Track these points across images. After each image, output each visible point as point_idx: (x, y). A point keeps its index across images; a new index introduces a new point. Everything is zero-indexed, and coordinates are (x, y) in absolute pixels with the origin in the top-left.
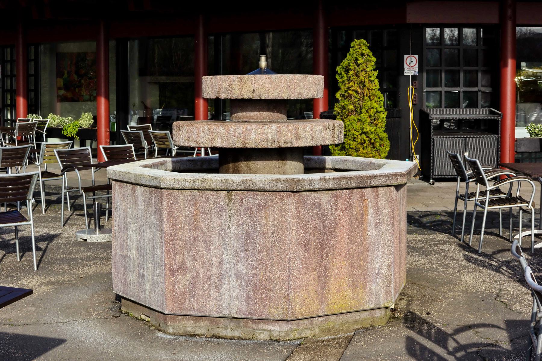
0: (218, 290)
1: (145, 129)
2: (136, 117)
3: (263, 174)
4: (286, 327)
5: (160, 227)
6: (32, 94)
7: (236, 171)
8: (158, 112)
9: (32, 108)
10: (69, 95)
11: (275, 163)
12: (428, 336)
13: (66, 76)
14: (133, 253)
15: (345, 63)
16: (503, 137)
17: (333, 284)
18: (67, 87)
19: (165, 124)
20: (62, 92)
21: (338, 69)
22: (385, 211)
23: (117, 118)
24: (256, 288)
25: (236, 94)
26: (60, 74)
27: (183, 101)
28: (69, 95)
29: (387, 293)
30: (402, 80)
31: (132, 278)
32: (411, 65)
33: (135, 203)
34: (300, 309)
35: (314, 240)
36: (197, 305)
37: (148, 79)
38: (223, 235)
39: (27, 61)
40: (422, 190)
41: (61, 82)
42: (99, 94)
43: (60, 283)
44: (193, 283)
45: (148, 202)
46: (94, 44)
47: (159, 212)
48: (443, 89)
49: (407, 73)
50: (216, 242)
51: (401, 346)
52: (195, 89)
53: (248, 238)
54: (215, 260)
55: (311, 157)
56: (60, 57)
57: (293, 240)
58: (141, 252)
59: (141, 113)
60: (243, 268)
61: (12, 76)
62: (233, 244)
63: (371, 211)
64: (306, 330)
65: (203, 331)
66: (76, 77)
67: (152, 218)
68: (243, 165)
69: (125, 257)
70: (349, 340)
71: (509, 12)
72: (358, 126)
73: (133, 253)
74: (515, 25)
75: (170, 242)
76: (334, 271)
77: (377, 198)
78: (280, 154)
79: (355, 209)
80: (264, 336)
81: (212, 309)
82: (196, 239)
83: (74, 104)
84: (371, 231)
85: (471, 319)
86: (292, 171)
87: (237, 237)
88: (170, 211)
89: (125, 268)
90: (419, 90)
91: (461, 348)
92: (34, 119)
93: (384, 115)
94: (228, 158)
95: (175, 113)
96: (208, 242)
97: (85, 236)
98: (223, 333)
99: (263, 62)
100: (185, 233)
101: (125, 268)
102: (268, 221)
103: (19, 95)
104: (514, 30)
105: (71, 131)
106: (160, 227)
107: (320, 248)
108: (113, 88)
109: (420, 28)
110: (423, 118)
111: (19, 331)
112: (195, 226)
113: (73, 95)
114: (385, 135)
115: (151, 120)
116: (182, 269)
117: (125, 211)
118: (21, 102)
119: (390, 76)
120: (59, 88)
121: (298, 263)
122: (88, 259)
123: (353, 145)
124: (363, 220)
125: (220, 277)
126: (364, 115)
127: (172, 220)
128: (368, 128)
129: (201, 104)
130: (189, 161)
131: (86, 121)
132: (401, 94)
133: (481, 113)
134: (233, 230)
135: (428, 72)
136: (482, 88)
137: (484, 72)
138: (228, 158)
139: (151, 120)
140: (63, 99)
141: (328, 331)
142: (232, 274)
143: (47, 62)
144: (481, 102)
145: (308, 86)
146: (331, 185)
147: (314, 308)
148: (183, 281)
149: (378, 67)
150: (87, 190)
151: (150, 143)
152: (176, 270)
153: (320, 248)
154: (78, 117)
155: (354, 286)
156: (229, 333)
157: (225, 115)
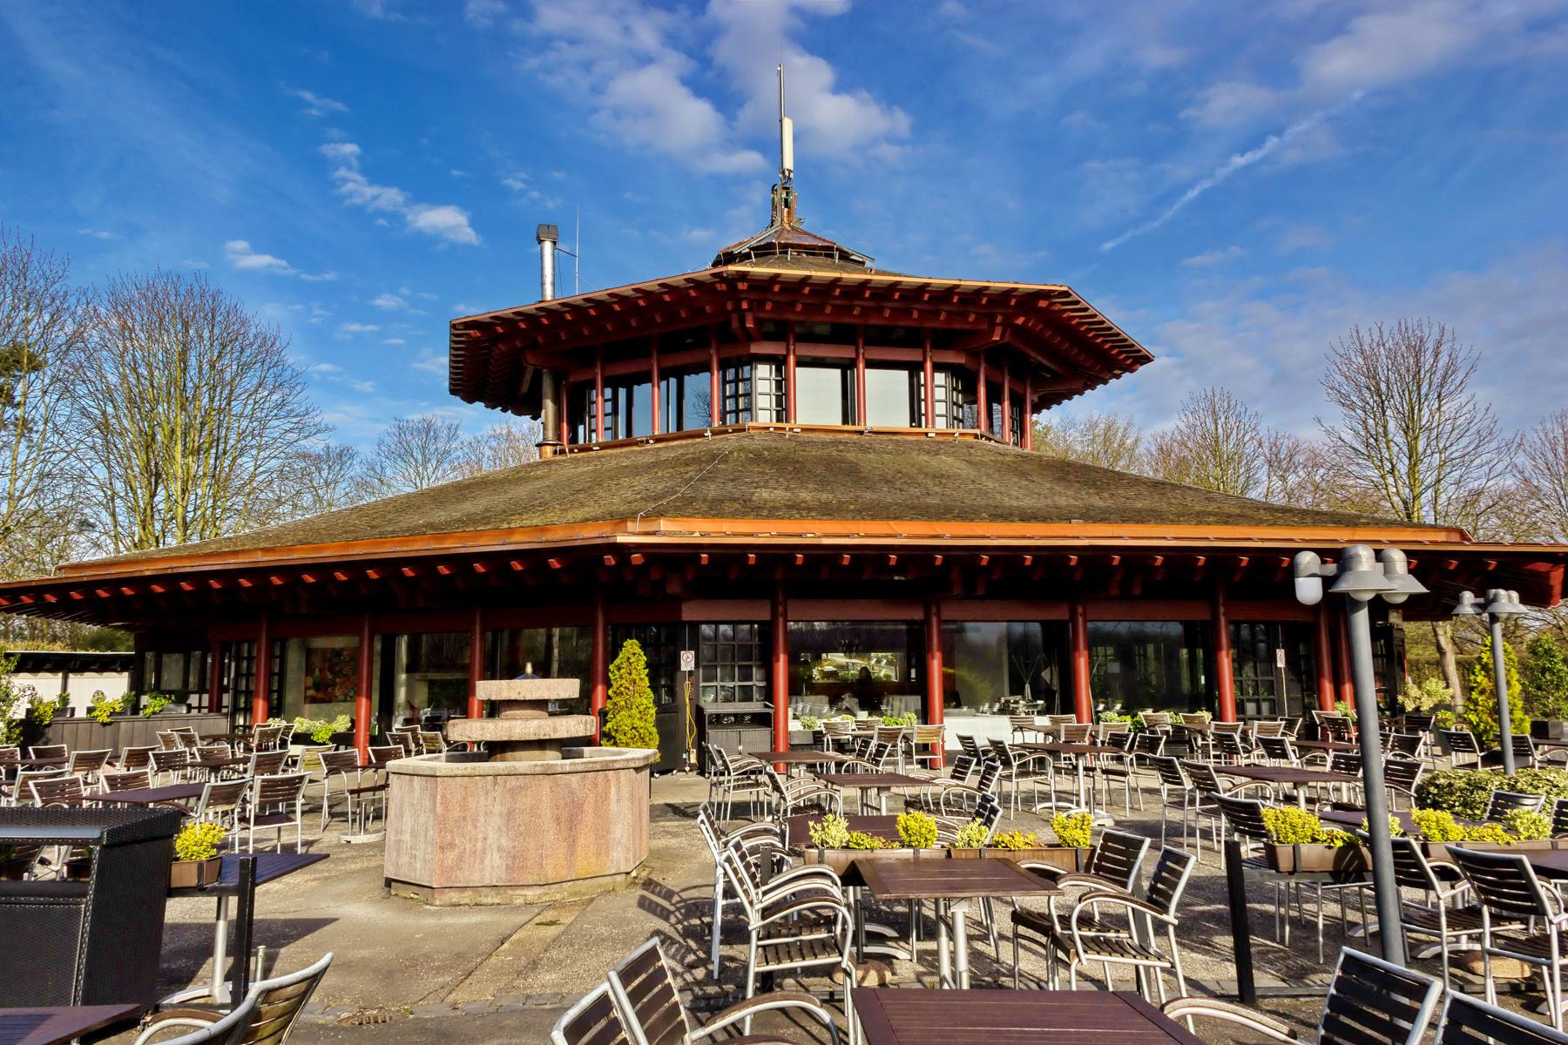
0: (482, 861)
1: (414, 731)
2: (401, 719)
3: (524, 762)
4: (539, 891)
5: (434, 810)
6: (275, 696)
7: (503, 760)
8: (426, 712)
9: (275, 711)
10: (321, 695)
11: (537, 753)
12: (659, 895)
13: (317, 672)
14: (407, 837)
15: (617, 662)
16: (776, 729)
18: (317, 687)
19: (435, 724)
20: (311, 692)
21: (611, 667)
22: (625, 790)
23: (379, 720)
24: (516, 860)
25: (504, 696)
26: (309, 671)
27: (455, 699)
28: (321, 695)
29: (627, 860)
30: (679, 675)
31: (405, 859)
32: (687, 660)
33: (412, 791)
34: (551, 875)
35: (564, 814)
37: (417, 676)
38: (488, 814)
39: (270, 657)
40: (696, 784)
41: (310, 681)
42: (358, 694)
43: (326, 879)
44: (460, 859)
45: (423, 790)
46: (356, 639)
47: (434, 798)
48: (718, 684)
49: (683, 668)
50: (482, 820)
51: (634, 902)
52: (471, 691)
53: (509, 815)
54: (480, 836)
55: (568, 746)
56: (309, 653)
57: (547, 813)
58: (414, 835)
59: (408, 714)
60: (504, 841)
61: (249, 675)
62: (496, 821)
63: (613, 790)
64: (556, 894)
65: (466, 901)
66: (330, 676)
67: (427, 803)
68: (509, 755)
69: (400, 841)
70: (592, 900)
72: (628, 722)
73: (407, 837)
75: (442, 823)
76: (581, 841)
77: (618, 780)
78: (541, 744)
79: (600, 789)
80: (519, 901)
82: (465, 819)
83: (325, 706)
84: (613, 806)
85: (699, 881)
86: (552, 758)
87: (501, 815)
88: (443, 796)
89: (398, 851)
90: (695, 685)
91: (683, 900)
92: (276, 723)
93: (653, 711)
94: (496, 749)
95: (444, 713)
96: (475, 821)
97: (348, 838)
98: (484, 900)
99: (529, 669)
100: (456, 814)
101: (398, 851)
103: (257, 696)
104: (785, 627)
105: (323, 736)
106: (434, 810)
107: (570, 819)
108: (376, 684)
109: (695, 626)
110: (699, 712)
111: (291, 916)
112: (464, 806)
113: (321, 696)
114: (654, 730)
115: (419, 721)
116: (452, 845)
117: (402, 800)
118: (260, 705)
119: (663, 672)
120: (307, 688)
121: (550, 834)
122: (353, 857)
123: (624, 739)
124: (607, 797)
125: (484, 852)
126: (634, 711)
127: (445, 803)
128: (638, 723)
129: (476, 708)
130: (460, 752)
131: (342, 724)
132: (678, 689)
133: (756, 707)
134: (497, 809)
135: (705, 667)
136: (757, 681)
137: (759, 667)
138: (496, 749)
139: (419, 721)
140: (313, 700)
141: (575, 894)
142: (494, 847)
143: (295, 659)
144: (756, 695)
145: (569, 688)
146: (580, 768)
147: (564, 874)
148: (451, 856)
149: (648, 665)
150: (352, 792)
151: (418, 745)
153: (570, 819)
154: (331, 720)
155: (598, 854)
156: (489, 900)
157: (1206, 947)
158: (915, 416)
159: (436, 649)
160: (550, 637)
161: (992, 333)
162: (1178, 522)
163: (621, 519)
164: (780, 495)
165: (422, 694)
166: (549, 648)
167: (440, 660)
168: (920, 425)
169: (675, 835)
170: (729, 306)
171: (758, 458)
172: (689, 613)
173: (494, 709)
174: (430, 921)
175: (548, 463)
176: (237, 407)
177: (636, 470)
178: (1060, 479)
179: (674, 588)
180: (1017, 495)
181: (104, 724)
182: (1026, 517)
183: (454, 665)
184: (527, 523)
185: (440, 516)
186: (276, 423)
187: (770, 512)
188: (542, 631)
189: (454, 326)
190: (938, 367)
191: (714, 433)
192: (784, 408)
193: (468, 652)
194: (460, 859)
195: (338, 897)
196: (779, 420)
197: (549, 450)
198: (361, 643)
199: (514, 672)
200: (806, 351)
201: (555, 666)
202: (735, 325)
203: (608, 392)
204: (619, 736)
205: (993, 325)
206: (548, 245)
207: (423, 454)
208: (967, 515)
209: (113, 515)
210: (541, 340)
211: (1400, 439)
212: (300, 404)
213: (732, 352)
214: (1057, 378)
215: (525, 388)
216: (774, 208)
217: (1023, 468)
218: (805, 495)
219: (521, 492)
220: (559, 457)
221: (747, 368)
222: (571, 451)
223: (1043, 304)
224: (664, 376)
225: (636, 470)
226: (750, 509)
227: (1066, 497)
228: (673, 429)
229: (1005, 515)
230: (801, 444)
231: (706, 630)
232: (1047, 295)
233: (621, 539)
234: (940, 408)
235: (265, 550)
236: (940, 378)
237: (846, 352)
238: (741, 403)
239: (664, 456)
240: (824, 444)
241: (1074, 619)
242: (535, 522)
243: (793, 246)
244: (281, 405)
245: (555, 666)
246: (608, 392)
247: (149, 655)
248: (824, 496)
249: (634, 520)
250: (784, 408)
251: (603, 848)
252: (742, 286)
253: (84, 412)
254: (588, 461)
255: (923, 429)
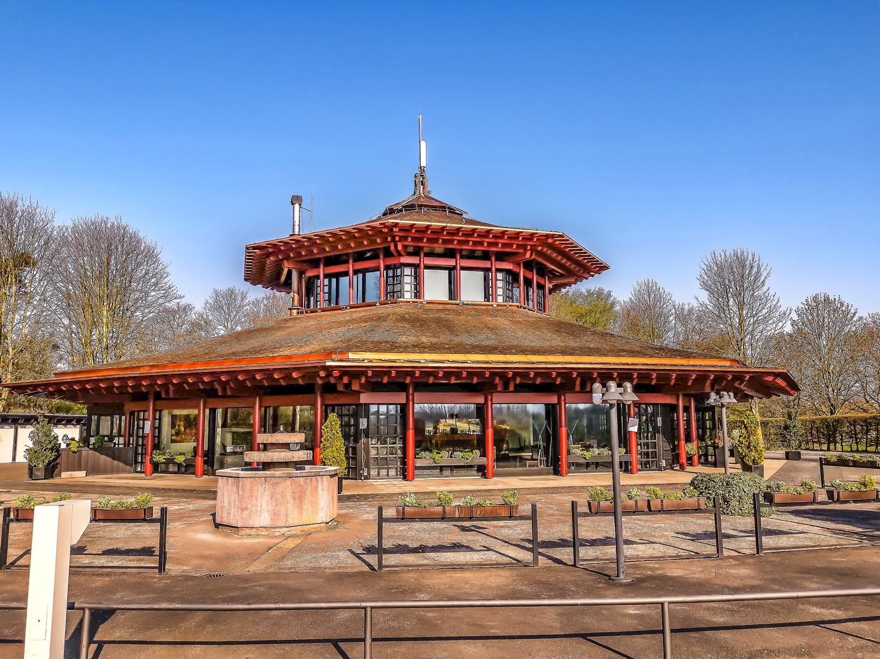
3: (278, 472)
14: (226, 504)
15: (326, 424)
17: (305, 513)
22: (326, 487)
24: (275, 515)
33: (228, 484)
34: (291, 523)
35: (297, 496)
36: (251, 523)
37: (227, 429)
44: (250, 514)
46: (404, 395)
55: (298, 465)
58: (229, 503)
60: (269, 507)
64: (294, 531)
71: (411, 397)
73: (226, 504)
74: (492, 404)
78: (286, 464)
81: (257, 524)
94: (266, 466)
102: (280, 489)
109: (367, 405)
116: (246, 509)
128: (336, 454)
138: (266, 466)
147: (297, 522)
148: (246, 513)
152: (243, 510)
158: (487, 297)
159: (235, 416)
160: (295, 410)
161: (525, 253)
162: (607, 356)
163: (329, 354)
164: (412, 339)
165: (229, 437)
166: (294, 415)
167: (239, 420)
168: (489, 301)
169: (352, 508)
170: (389, 239)
171: (403, 319)
172: (364, 398)
173: (266, 447)
174: (237, 541)
175: (295, 319)
176: (134, 285)
177: (340, 324)
178: (557, 331)
179: (355, 387)
180: (532, 339)
181: (74, 452)
182: (535, 352)
183: (245, 422)
184: (283, 353)
185: (238, 348)
186: (153, 293)
187: (405, 349)
188: (291, 408)
189: (247, 248)
190: (498, 270)
191: (381, 304)
192: (418, 293)
193: (251, 418)
194: (250, 514)
195: (196, 532)
196: (416, 297)
197: (295, 311)
198: (199, 412)
199: (275, 429)
200: (429, 261)
201: (298, 426)
202: (392, 248)
203: (326, 281)
204: (326, 461)
205: (526, 250)
206: (297, 206)
207: (229, 309)
208: (504, 351)
209: (71, 343)
210: (292, 255)
211: (735, 309)
212: (166, 283)
213: (391, 261)
214: (570, 273)
215: (283, 278)
216: (416, 185)
217: (536, 325)
218: (424, 339)
219: (279, 334)
220: (300, 316)
221: (399, 270)
222: (307, 312)
223: (550, 241)
224: (356, 272)
225: (340, 324)
226: (394, 347)
227: (558, 341)
228: (360, 302)
229: (524, 351)
230: (425, 310)
231: (373, 408)
232: (553, 236)
233: (328, 364)
234: (500, 292)
235: (153, 366)
236: (500, 276)
237: (451, 262)
238: (392, 294)
239: (355, 316)
240: (438, 311)
241: (559, 403)
242: (287, 353)
243: (425, 206)
244: (156, 284)
245: (298, 426)
246: (326, 281)
247: (94, 418)
248: (434, 340)
249: (335, 353)
250: (418, 292)
251: (315, 512)
252: (396, 230)
253: (59, 290)
254: (315, 318)
255: (491, 303)
